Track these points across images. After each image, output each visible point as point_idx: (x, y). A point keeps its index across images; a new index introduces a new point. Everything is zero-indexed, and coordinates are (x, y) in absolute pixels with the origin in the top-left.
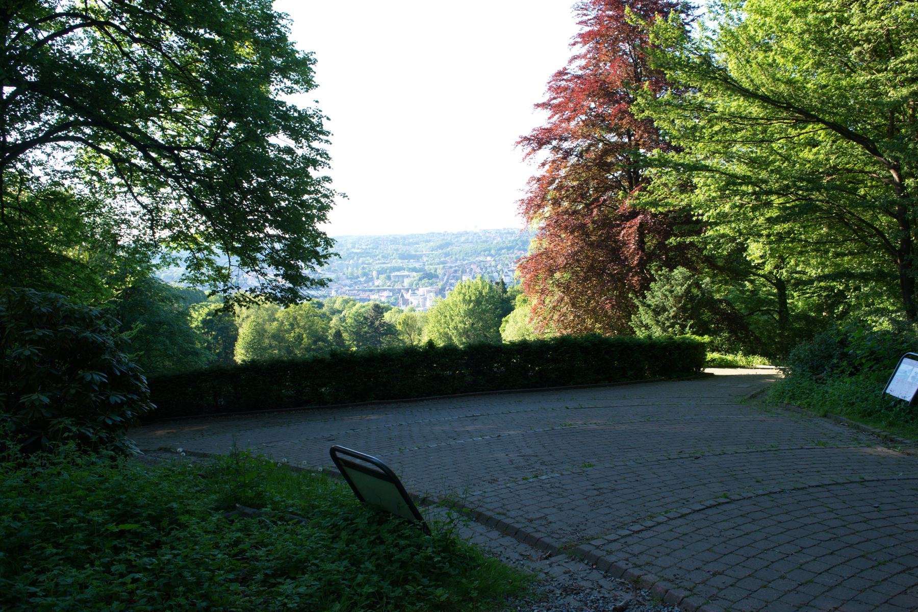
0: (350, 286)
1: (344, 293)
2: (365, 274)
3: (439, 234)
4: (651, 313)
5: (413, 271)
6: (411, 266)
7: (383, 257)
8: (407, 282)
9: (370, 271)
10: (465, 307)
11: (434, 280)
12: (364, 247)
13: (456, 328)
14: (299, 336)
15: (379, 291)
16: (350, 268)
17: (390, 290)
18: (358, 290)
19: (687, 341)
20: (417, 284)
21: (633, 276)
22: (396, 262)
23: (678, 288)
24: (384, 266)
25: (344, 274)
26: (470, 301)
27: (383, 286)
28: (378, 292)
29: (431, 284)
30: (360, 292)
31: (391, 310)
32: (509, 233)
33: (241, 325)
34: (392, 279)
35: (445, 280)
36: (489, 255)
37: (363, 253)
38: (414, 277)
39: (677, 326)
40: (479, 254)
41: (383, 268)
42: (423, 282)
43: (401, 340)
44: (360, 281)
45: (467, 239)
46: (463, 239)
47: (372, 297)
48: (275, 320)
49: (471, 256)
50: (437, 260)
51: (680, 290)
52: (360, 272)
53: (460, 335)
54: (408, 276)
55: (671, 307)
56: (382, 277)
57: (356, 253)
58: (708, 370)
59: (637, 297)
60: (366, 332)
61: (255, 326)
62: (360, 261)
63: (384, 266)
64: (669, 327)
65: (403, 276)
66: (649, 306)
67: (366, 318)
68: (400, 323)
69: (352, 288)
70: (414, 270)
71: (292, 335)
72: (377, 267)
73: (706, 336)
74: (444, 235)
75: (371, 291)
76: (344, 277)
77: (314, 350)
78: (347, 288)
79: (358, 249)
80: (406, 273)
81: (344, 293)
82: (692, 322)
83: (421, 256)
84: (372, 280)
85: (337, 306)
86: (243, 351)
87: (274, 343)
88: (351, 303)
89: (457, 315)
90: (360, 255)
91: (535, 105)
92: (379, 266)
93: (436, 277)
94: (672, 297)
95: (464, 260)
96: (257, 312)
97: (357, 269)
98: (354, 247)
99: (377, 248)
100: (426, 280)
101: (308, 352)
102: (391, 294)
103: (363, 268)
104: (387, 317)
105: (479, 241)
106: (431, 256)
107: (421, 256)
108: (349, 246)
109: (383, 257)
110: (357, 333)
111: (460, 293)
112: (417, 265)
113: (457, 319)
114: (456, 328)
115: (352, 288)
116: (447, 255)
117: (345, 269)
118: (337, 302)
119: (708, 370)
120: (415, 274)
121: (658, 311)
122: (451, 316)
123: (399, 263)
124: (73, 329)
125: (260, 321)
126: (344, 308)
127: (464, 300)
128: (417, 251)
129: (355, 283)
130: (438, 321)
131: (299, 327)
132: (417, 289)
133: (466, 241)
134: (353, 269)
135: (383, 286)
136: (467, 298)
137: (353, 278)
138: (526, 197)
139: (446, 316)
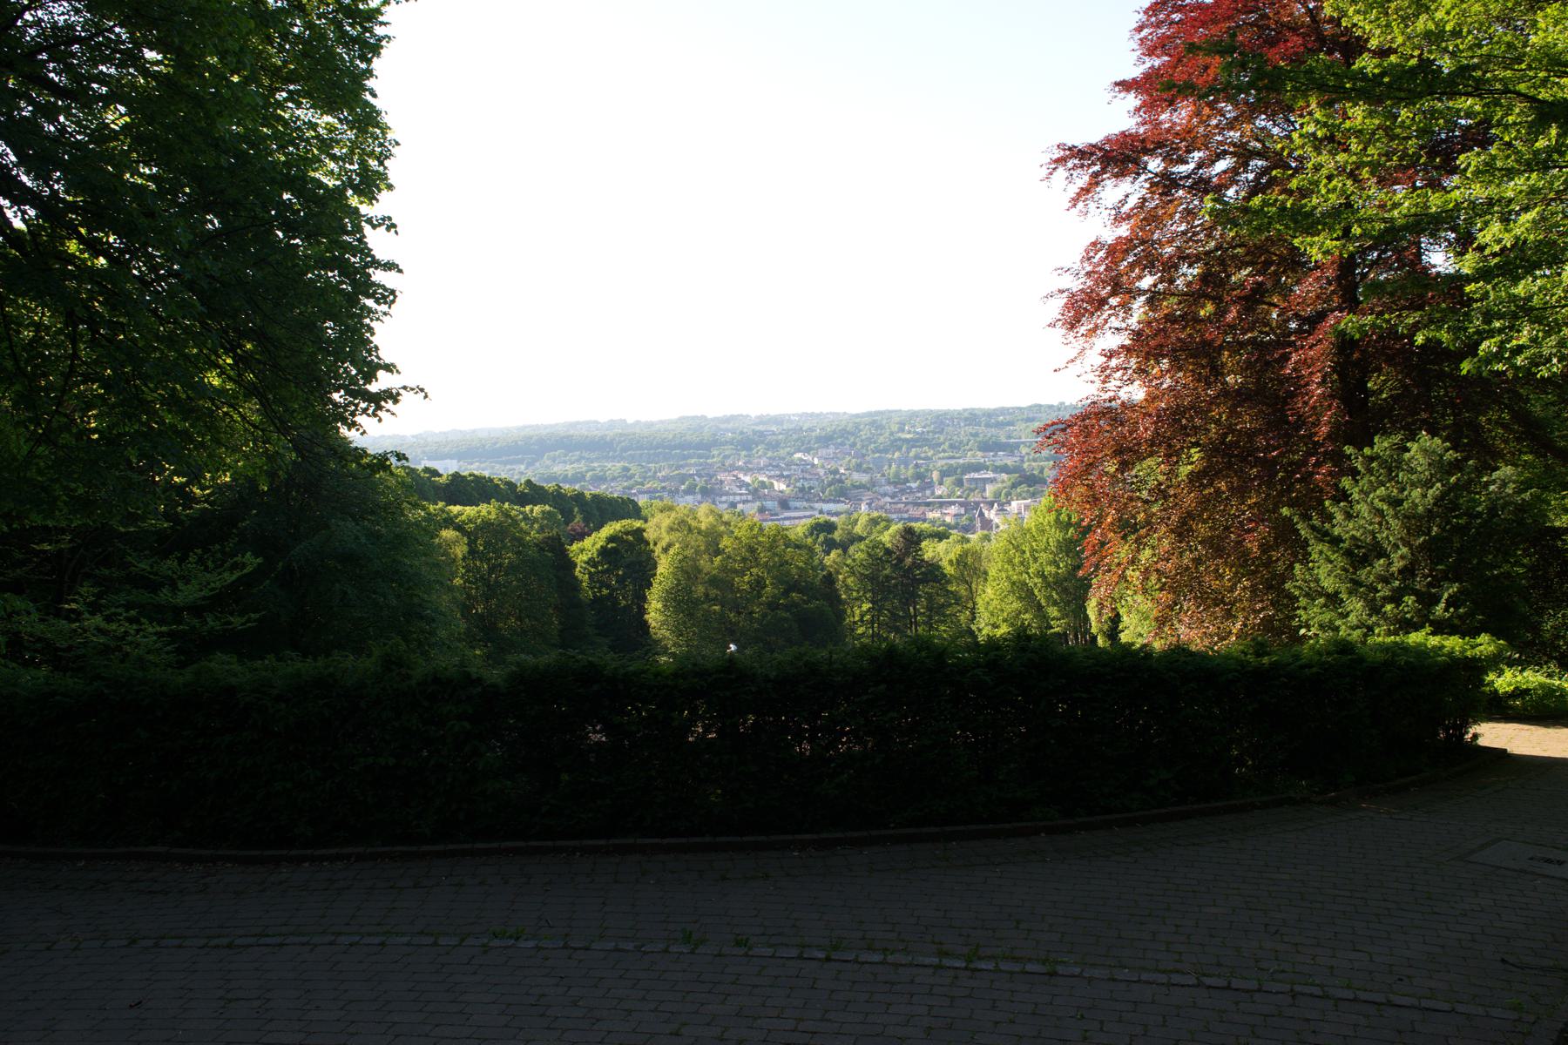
0: (892, 497)
1: (882, 508)
2: (919, 476)
3: (1051, 407)
4: (1340, 561)
5: (1002, 471)
6: (998, 464)
7: (952, 447)
8: (990, 490)
9: (927, 470)
10: (1059, 535)
11: (1038, 487)
12: (919, 430)
13: (1041, 574)
15: (941, 505)
17: (961, 504)
18: (906, 504)
19: (1402, 660)
20: (1008, 494)
21: (1318, 464)
22: (973, 456)
23: (1417, 492)
24: (952, 462)
25: (883, 475)
26: (1069, 524)
27: (949, 496)
29: (1033, 495)
30: (910, 507)
31: (948, 538)
38: (1003, 482)
39: (1410, 600)
42: (1019, 490)
43: (952, 592)
44: (910, 488)
47: (931, 515)
48: (718, 552)
51: (1419, 498)
52: (911, 472)
53: (1048, 585)
54: (992, 481)
55: (1396, 547)
56: (948, 481)
58: (1492, 734)
59: (1306, 517)
61: (680, 561)
62: (911, 454)
63: (952, 462)
64: (1386, 600)
65: (985, 481)
66: (1335, 541)
67: (888, 552)
68: (951, 562)
69: (896, 500)
70: (1005, 469)
71: (746, 578)
73: (1484, 638)
74: (1059, 409)
76: (883, 480)
78: (888, 499)
79: (909, 432)
80: (990, 475)
81: (882, 508)
82: (1455, 588)
83: (1017, 446)
84: (930, 485)
85: (858, 529)
86: (659, 606)
87: (713, 592)
88: (883, 524)
89: (1045, 550)
90: (912, 443)
91: (1117, 84)
92: (944, 462)
93: (1043, 482)
94: (1396, 516)
97: (906, 467)
98: (902, 430)
99: (941, 432)
100: (1024, 487)
102: (962, 511)
103: (917, 466)
104: (931, 550)
107: (1017, 446)
108: (895, 428)
109: (952, 447)
110: (872, 578)
111: (1050, 511)
112: (1009, 461)
113: (1043, 557)
114: (1041, 574)
115: (896, 500)
117: (886, 467)
118: (859, 523)
119: (1492, 734)
120: (1004, 476)
121: (1361, 555)
122: (1033, 550)
123: (979, 457)
125: (689, 552)
126: (870, 533)
127: (1057, 520)
128: (1010, 437)
129: (903, 492)
130: (1010, 561)
132: (1009, 503)
134: (899, 467)
136: (1064, 517)
137: (898, 482)
138: (1076, 285)
139: (1024, 552)
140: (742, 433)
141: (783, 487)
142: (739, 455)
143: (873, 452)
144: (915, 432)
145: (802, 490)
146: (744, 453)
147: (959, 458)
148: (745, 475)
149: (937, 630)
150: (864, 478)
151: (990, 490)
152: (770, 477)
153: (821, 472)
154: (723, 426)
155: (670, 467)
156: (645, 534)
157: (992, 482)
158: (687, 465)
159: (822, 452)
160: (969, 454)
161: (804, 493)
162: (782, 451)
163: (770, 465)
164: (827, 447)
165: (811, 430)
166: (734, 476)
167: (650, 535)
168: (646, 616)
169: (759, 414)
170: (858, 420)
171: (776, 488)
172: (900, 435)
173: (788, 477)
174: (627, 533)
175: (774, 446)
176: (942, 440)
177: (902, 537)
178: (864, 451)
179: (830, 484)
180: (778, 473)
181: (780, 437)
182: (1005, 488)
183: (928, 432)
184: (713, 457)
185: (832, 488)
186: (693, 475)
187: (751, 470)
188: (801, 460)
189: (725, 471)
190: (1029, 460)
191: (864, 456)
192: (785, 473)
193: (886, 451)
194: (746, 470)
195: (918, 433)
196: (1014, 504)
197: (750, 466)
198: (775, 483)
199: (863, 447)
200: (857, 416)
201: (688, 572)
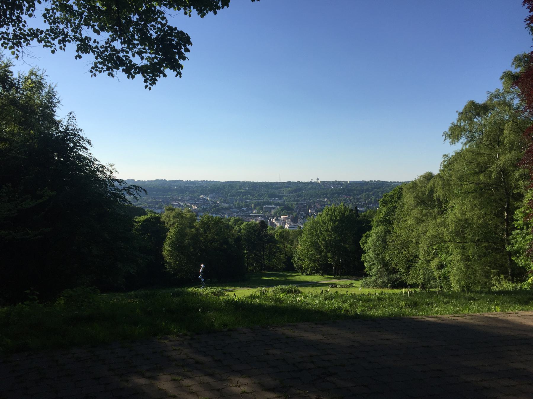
6: (276, 202)
7: (259, 195)
8: (273, 212)
9: (250, 204)
17: (262, 217)
18: (242, 216)
29: (289, 214)
32: (339, 184)
34: (264, 209)
35: (298, 211)
36: (326, 197)
38: (278, 209)
40: (319, 197)
44: (243, 210)
45: (312, 187)
46: (309, 187)
49: (314, 197)
50: (292, 199)
52: (244, 204)
54: (274, 208)
56: (257, 208)
62: (244, 197)
63: (259, 201)
67: (255, 231)
69: (238, 214)
72: (254, 201)
78: (235, 214)
79: (243, 190)
80: (273, 206)
83: (282, 196)
90: (244, 194)
92: (256, 201)
95: (310, 200)
97: (242, 202)
103: (246, 202)
105: (319, 188)
106: (289, 196)
108: (238, 188)
109: (259, 195)
111: (328, 215)
112: (279, 201)
113: (326, 233)
115: (238, 214)
116: (299, 196)
118: (231, 221)
122: (321, 231)
127: (331, 219)
129: (241, 211)
133: (312, 188)
137: (239, 207)
140: (180, 187)
141: (196, 207)
142: (179, 195)
143: (230, 196)
144: (245, 189)
145: (203, 209)
146: (181, 194)
147: (261, 200)
148: (182, 203)
149: (272, 261)
150: (226, 205)
151: (273, 212)
152: (191, 204)
153: (211, 203)
154: (173, 184)
155: (152, 198)
156: (161, 220)
157: (274, 209)
158: (160, 198)
159: (211, 195)
160: (265, 198)
161: (204, 210)
162: (195, 194)
163: (191, 199)
164: (213, 194)
165: (207, 187)
166: (177, 203)
167: (163, 218)
168: (163, 253)
169: (186, 180)
170: (224, 184)
171: (193, 208)
172: (240, 190)
173: (198, 204)
174: (152, 218)
175: (193, 192)
176: (255, 193)
177: (260, 225)
178: (226, 196)
179: (214, 207)
180: (194, 202)
181: (195, 189)
182: (279, 211)
183: (250, 190)
184: (169, 195)
185: (215, 209)
186: (161, 202)
187: (184, 201)
188: (202, 197)
189: (174, 201)
190: (287, 202)
191: (226, 197)
192: (197, 203)
193: (234, 196)
194: (181, 201)
195: (246, 190)
196: (282, 217)
197: (183, 199)
198: (193, 206)
199: (226, 194)
200: (224, 182)
201: (181, 234)
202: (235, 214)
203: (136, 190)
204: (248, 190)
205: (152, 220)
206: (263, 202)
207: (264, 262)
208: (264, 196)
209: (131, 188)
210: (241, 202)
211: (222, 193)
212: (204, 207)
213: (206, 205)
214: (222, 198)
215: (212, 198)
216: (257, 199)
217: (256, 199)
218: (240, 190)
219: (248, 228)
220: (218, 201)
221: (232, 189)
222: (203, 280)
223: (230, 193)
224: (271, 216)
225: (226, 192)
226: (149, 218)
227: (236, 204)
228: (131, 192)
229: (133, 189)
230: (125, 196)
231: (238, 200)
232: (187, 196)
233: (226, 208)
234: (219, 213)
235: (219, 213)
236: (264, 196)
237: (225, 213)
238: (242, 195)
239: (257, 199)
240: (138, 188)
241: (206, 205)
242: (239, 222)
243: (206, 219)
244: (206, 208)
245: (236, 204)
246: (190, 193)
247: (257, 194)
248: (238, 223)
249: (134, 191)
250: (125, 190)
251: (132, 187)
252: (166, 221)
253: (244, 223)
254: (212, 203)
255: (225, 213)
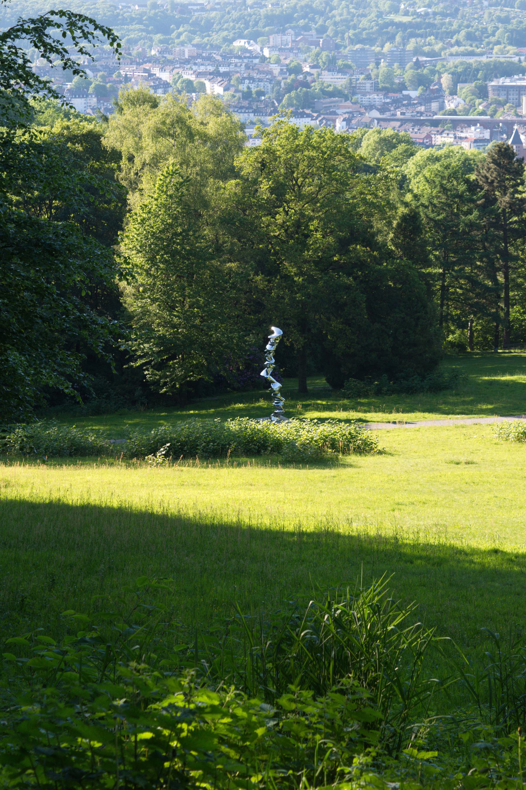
0: (383, 109)
7: (470, 37)
9: (433, 72)
14: (298, 225)
15: (455, 125)
16: (383, 64)
17: (485, 125)
18: (403, 122)
22: (502, 52)
24: (472, 60)
25: (368, 77)
27: (467, 112)
28: (454, 128)
33: (134, 185)
34: (491, 95)
37: (418, 26)
41: (469, 65)
44: (408, 98)
47: (438, 140)
52: (409, 74)
56: (465, 89)
57: (400, 26)
60: (471, 225)
62: (411, 46)
63: (472, 60)
67: (473, 187)
69: (387, 115)
71: (280, 218)
72: (452, 62)
75: (435, 123)
77: (338, 267)
78: (375, 114)
79: (406, 13)
88: (402, 147)
92: (458, 60)
96: (183, 146)
97: (402, 66)
98: (395, 10)
99: (454, 14)
101: (324, 271)
102: (487, 134)
103: (418, 65)
109: (470, 37)
115: (387, 115)
117: (371, 66)
118: (364, 144)
124: (490, 407)
125: (192, 172)
129: (397, 103)
131: (300, 197)
134: (390, 65)
135: (467, 112)
141: (219, 90)
142: (151, 40)
143: (352, 42)
144: (415, 13)
145: (247, 95)
146: (158, 37)
147: (481, 54)
148: (162, 69)
152: (199, 75)
153: (276, 69)
156: (104, 142)
159: (276, 39)
160: (496, 48)
162: (215, 36)
163: (199, 56)
164: (283, 32)
166: (145, 71)
171: (209, 91)
172: (392, 16)
173: (227, 75)
174: (73, 139)
177: (494, 162)
178: (338, 41)
179: (289, 89)
180: (211, 69)
181: (213, 14)
183: (435, 14)
185: (293, 94)
187: (171, 62)
188: (244, 50)
191: (337, 47)
192: (222, 69)
193: (371, 41)
195: (419, 15)
197: (169, 57)
198: (208, 84)
199: (336, 34)
202: (375, 114)
203: (72, 32)
204: (427, 14)
205: (69, 144)
206: (487, 65)
207: (508, 314)
208: (493, 39)
209: (50, 23)
210: (396, 65)
211: (322, 30)
212: (252, 86)
213: (260, 80)
214: (323, 49)
215: (280, 50)
216: (464, 54)
217: (457, 55)
218: (392, 16)
219: (443, 178)
220: (305, 61)
221: (361, 11)
222: (276, 386)
223: (355, 27)
224: (520, 123)
225: (335, 24)
226: (61, 135)
227: (377, 76)
228: (48, 41)
229: (59, 26)
230: (26, 61)
231: (384, 56)
232: (182, 44)
233: (336, 93)
234: (308, 111)
235: (308, 111)
236: (493, 39)
237: (335, 113)
238: (403, 39)
239: (464, 54)
240: (80, 24)
241: (260, 80)
242: (394, 147)
243: (284, 142)
244: (260, 93)
245: (377, 76)
246: (194, 33)
247: (463, 33)
248: (394, 152)
249: (64, 35)
250: (27, 32)
251: (55, 18)
252: (123, 149)
253: (418, 154)
254: (282, 72)
255: (335, 113)
